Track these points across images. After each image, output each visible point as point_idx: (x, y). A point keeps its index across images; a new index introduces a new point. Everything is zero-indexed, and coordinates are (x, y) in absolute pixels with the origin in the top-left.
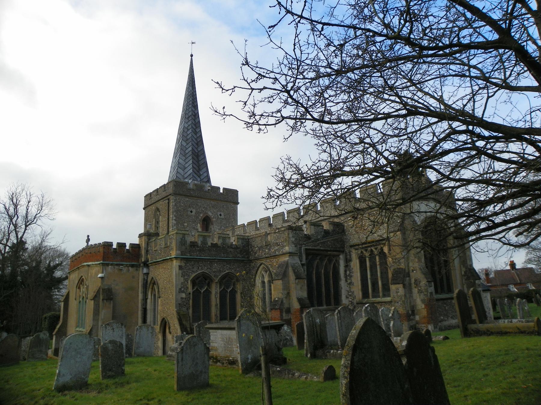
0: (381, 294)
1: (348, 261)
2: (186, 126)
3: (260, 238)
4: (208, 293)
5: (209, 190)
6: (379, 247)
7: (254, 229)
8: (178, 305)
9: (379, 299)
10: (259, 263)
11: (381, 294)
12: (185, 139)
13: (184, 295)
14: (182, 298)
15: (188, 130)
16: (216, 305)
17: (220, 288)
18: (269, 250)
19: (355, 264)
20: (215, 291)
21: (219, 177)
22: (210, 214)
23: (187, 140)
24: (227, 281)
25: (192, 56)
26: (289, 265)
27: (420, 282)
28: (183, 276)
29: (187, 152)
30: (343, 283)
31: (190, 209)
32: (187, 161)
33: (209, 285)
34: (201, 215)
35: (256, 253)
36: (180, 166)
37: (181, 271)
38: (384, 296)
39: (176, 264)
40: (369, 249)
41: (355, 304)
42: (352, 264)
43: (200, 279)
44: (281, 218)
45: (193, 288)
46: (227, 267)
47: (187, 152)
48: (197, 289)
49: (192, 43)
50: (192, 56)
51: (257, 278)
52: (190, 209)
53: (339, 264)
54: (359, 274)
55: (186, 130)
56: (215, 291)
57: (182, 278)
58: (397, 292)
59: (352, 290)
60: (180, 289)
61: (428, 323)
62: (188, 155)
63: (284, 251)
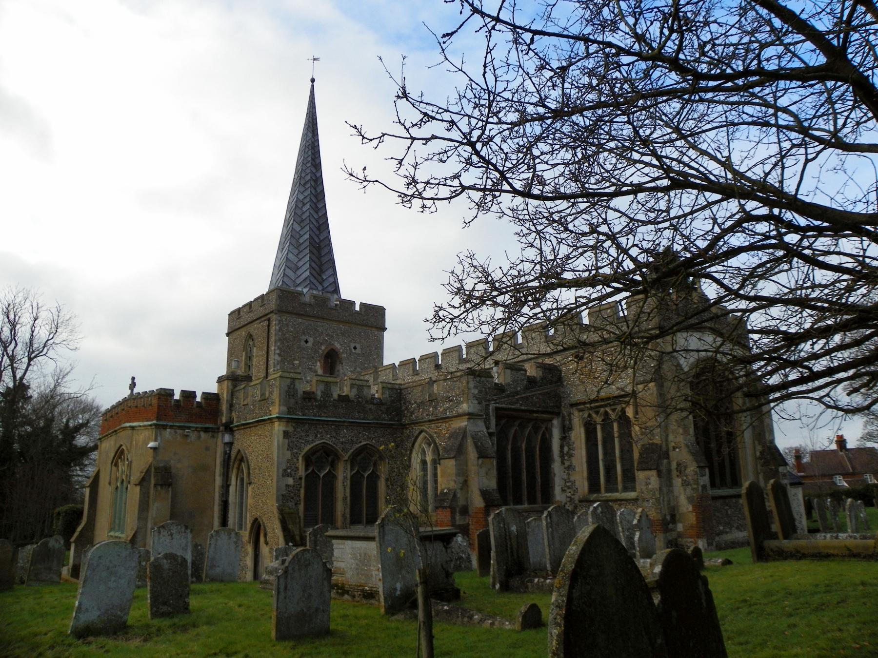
0: (620, 487)
1: (566, 429)
2: (301, 197)
3: (420, 388)
4: (331, 478)
5: (336, 305)
6: (619, 408)
7: (411, 372)
8: (281, 498)
9: (616, 495)
10: (417, 429)
11: (620, 487)
12: (299, 220)
13: (290, 481)
14: (287, 486)
15: (304, 204)
16: (345, 498)
17: (352, 470)
18: (435, 408)
19: (578, 434)
20: (343, 474)
21: (355, 284)
22: (337, 345)
23: (303, 221)
24: (364, 458)
25: (313, 80)
26: (468, 434)
27: (686, 467)
28: (290, 448)
29: (301, 241)
30: (557, 467)
31: (304, 338)
32: (300, 256)
33: (333, 465)
34: (323, 348)
35: (412, 413)
36: (288, 264)
37: (286, 441)
38: (626, 489)
39: (278, 428)
40: (602, 410)
41: (577, 502)
42: (573, 435)
43: (318, 454)
44: (456, 355)
45: (306, 470)
46: (364, 435)
47: (301, 241)
48: (313, 470)
49: (314, 59)
50: (313, 80)
51: (414, 455)
52: (304, 338)
53: (551, 435)
54: (584, 452)
55: (300, 205)
56: (343, 474)
57: (289, 453)
58: (647, 484)
59: (572, 478)
60: (285, 470)
61: (698, 537)
62: (303, 247)
63: (460, 411)
